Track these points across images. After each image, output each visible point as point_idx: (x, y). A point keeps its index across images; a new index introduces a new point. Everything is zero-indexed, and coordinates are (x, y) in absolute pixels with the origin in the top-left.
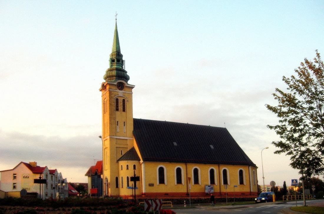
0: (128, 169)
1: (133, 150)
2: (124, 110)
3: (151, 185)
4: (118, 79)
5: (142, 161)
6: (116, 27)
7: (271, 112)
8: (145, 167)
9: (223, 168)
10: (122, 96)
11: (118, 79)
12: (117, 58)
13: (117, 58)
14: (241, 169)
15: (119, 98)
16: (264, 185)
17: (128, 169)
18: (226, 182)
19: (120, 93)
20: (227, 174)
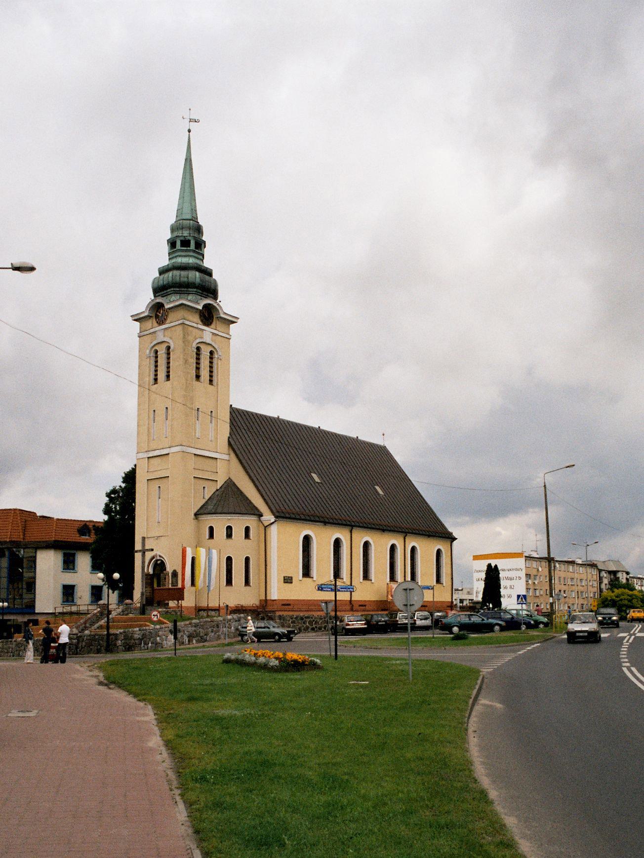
0: (247, 536)
1: (230, 486)
2: (211, 381)
3: (288, 580)
4: (186, 286)
5: (268, 517)
6: (188, 161)
7: (17, 272)
8: (279, 533)
9: (412, 542)
10: (210, 342)
11: (186, 286)
12: (188, 238)
13: (188, 238)
14: (441, 548)
15: (202, 346)
16: (351, 601)
17: (247, 536)
18: (413, 577)
19: (207, 333)
20: (135, 574)
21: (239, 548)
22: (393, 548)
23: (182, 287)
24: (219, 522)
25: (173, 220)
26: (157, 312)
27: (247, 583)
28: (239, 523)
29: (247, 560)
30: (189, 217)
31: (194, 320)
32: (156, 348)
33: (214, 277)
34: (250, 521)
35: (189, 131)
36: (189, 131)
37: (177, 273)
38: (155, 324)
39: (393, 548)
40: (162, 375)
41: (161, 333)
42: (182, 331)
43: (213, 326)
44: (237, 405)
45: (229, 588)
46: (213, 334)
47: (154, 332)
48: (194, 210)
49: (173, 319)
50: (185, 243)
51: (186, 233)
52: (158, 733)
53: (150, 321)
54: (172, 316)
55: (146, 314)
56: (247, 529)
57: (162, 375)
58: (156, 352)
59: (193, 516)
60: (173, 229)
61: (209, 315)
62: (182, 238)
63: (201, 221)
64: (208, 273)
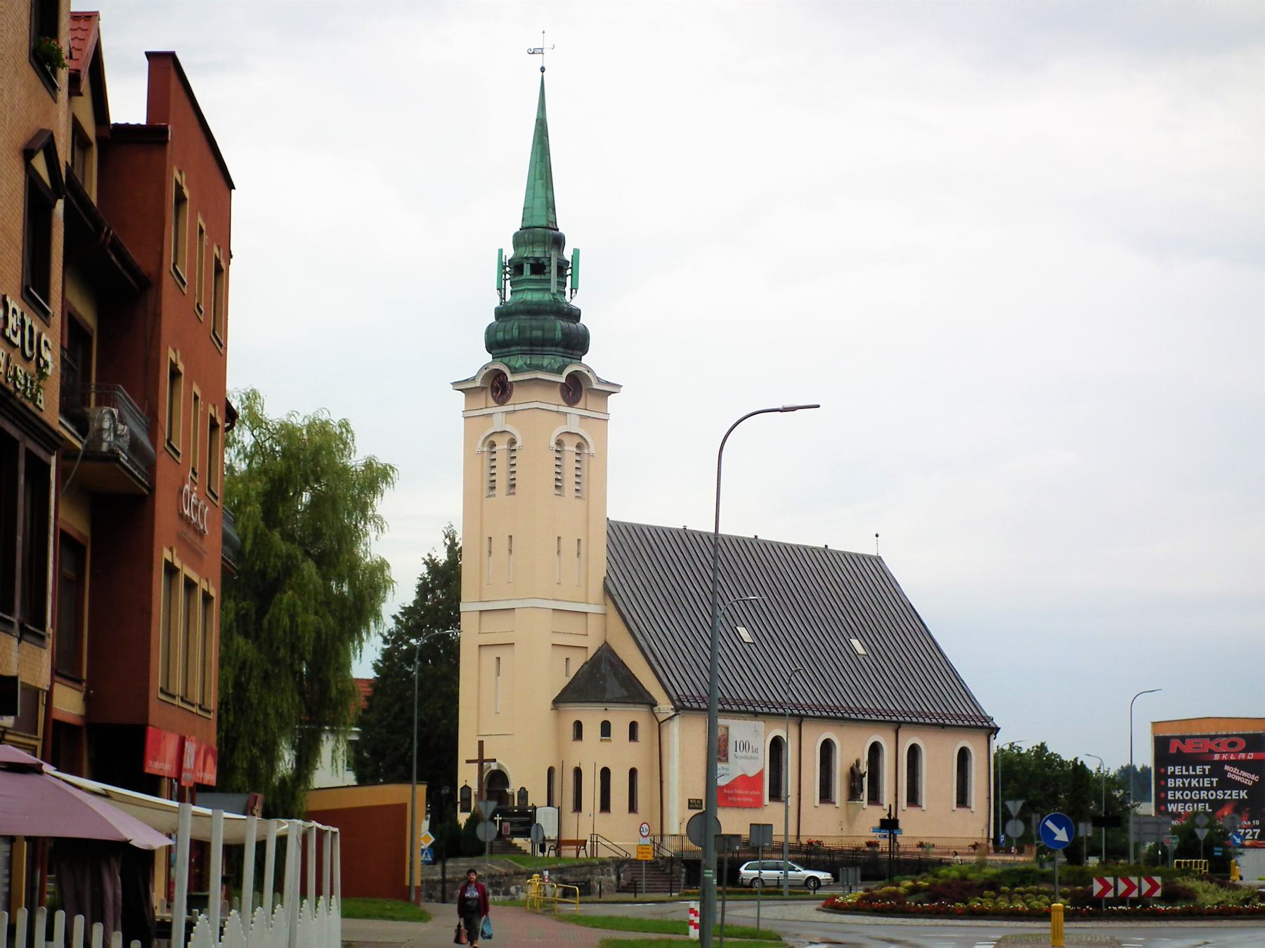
11: (537, 334)
12: (539, 257)
13: (539, 257)
15: (565, 439)
17: (633, 736)
19: (574, 418)
21: (620, 755)
22: (963, 755)
23: (533, 345)
24: (591, 717)
25: (517, 226)
26: (497, 386)
27: (632, 808)
28: (620, 718)
29: (633, 773)
30: (543, 222)
31: (554, 400)
32: (492, 438)
33: (584, 320)
34: (638, 714)
35: (543, 70)
36: (543, 70)
37: (525, 321)
38: (492, 402)
39: (963, 755)
40: (502, 483)
41: (499, 418)
42: (536, 415)
43: (581, 404)
44: (614, 517)
45: (605, 815)
46: (581, 416)
47: (491, 415)
48: (550, 206)
49: (518, 399)
50: (539, 268)
51: (538, 253)
52: (640, 858)
53: (483, 396)
54: (517, 395)
55: (478, 384)
56: (633, 726)
57: (502, 483)
58: (493, 445)
59: (549, 705)
60: (518, 241)
61: (575, 388)
62: (704, 862)
63: (563, 227)
64: (574, 315)
